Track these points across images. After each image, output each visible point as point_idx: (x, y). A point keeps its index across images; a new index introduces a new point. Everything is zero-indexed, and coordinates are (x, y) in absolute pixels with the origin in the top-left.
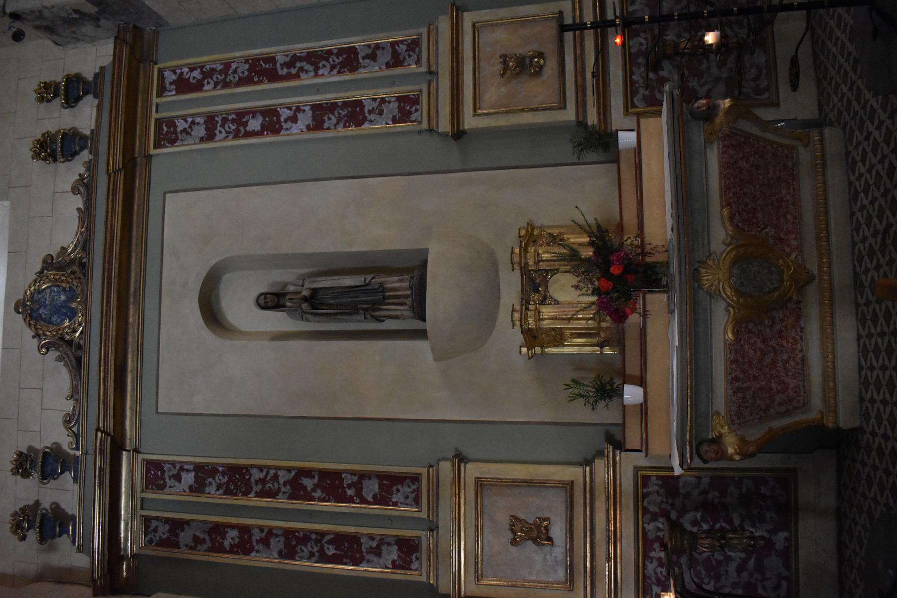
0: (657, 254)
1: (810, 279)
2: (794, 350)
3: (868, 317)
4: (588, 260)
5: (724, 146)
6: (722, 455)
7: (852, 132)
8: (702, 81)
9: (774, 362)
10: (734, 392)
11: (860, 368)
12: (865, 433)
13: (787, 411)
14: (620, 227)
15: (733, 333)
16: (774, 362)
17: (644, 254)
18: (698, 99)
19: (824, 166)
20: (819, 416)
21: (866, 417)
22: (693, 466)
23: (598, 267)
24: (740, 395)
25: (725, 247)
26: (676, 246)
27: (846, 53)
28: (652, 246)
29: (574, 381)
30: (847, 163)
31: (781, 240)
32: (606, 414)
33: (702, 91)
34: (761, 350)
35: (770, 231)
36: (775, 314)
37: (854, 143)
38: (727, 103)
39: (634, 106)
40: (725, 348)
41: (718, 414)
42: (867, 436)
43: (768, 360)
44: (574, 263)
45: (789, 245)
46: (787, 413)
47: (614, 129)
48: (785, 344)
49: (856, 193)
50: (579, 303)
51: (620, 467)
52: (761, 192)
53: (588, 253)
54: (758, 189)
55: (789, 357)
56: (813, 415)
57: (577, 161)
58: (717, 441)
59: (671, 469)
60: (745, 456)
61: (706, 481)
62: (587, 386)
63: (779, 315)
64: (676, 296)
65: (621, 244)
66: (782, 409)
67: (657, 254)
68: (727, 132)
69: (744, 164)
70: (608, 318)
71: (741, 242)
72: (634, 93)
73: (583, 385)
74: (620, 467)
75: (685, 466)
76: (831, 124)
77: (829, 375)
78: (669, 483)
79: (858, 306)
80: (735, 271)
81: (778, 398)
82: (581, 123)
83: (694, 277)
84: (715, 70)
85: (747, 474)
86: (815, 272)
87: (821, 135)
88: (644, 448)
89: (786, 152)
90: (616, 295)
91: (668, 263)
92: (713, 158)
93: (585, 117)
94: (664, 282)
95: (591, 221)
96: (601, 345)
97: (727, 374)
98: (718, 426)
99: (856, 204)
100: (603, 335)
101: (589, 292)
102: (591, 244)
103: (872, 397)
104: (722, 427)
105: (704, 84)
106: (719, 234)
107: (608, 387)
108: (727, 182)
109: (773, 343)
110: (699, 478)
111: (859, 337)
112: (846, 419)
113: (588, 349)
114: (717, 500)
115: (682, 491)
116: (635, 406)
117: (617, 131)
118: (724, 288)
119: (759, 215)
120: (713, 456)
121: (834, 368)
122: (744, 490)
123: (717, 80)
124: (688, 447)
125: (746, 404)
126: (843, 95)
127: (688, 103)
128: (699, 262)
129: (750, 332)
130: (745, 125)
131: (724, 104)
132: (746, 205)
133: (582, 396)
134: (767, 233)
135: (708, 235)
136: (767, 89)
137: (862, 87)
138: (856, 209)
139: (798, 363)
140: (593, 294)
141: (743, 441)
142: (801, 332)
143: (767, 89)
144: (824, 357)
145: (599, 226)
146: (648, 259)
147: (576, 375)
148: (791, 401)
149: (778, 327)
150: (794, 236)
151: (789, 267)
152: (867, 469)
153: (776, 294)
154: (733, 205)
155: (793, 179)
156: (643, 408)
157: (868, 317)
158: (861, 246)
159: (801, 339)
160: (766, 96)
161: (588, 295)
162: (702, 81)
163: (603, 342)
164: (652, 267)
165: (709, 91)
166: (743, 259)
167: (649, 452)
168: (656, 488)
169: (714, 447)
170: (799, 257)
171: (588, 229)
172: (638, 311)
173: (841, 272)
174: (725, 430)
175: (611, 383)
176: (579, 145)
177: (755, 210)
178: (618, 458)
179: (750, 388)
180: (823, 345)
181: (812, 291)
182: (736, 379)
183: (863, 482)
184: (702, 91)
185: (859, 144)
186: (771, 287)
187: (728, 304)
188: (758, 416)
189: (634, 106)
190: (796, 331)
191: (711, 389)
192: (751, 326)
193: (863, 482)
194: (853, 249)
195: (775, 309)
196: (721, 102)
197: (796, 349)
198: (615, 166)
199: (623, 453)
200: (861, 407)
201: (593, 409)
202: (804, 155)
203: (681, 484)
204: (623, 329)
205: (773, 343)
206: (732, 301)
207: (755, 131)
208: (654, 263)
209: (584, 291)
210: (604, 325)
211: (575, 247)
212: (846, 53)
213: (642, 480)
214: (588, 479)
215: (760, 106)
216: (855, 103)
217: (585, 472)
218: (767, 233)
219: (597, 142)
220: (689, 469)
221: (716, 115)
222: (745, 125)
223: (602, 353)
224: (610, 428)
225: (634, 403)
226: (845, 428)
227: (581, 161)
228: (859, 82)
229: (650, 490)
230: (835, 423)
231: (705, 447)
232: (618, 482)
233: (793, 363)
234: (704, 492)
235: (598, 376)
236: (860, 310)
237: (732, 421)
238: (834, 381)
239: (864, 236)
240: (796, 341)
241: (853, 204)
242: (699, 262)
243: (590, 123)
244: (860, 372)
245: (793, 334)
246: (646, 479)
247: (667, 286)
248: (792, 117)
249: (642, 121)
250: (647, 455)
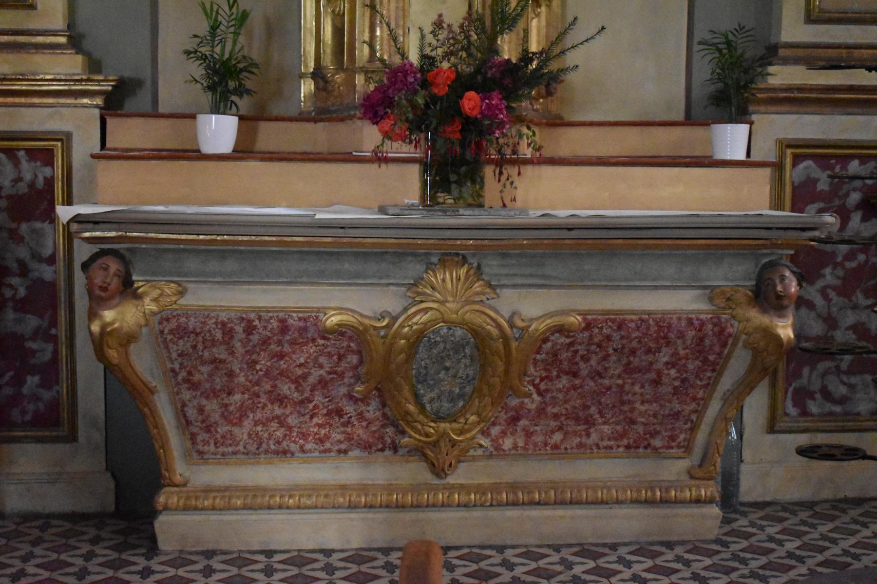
0: (499, 186)
1: (438, 471)
2: (304, 436)
3: (364, 568)
4: (494, 50)
5: (702, 324)
6: (99, 299)
7: (711, 554)
8: (832, 294)
9: (281, 400)
10: (224, 324)
11: (269, 553)
12: (148, 559)
13: (188, 423)
14: (556, 122)
15: (339, 325)
16: (281, 400)
17: (500, 163)
18: (801, 279)
19: (650, 502)
20: (178, 479)
21: (181, 560)
22: (76, 242)
23: (478, 71)
24: (219, 335)
25: (507, 316)
26: (512, 221)
27: (858, 551)
28: (515, 178)
29: (244, 16)
30: (652, 544)
31: (515, 420)
32: (177, 79)
33: (812, 293)
34: (305, 377)
35: (533, 403)
36: (374, 404)
37: (687, 556)
38: (785, 330)
39: (797, 159)
40: (311, 309)
41: (182, 293)
42: (142, 562)
43: (286, 388)
44: (488, 23)
45: (504, 433)
46: (184, 422)
47: (754, 117)
48: (315, 420)
49: (595, 556)
50: (407, 32)
51: (68, 106)
52: (609, 388)
53: (508, 48)
54: (613, 384)
55: (290, 428)
56: (180, 469)
57: (696, 40)
58: (127, 288)
59: (69, 201)
60: (99, 344)
61: (47, 272)
62: (235, 42)
63: (372, 410)
64: (416, 218)
65: (520, 120)
66: (192, 413)
67: (499, 186)
68: (730, 330)
69: (664, 357)
70: (372, 87)
71: (514, 345)
72: (822, 161)
73: (236, 34)
74: (68, 106)
75: (74, 227)
76: (726, 521)
77: (257, 500)
78: (37, 203)
79: (386, 551)
80: (459, 332)
81: (212, 406)
82: (772, 53)
83: (452, 257)
84: (850, 318)
85: (64, 351)
86: (451, 480)
87: (710, 501)
88: (106, 152)
89: (682, 437)
90: (420, 101)
91: (481, 206)
92: (682, 302)
93: (785, 61)
94: (441, 197)
95: (571, 59)
96: (318, 74)
97: (258, 311)
98: (155, 293)
99: (575, 554)
100: (339, 78)
101: (427, 51)
102: (526, 57)
103: (215, 571)
104: (155, 300)
105: (825, 296)
106: (533, 306)
107: (232, 84)
108: (632, 325)
109: (319, 399)
110: (51, 260)
111: (328, 553)
112: (172, 527)
113: (310, 47)
114: (8, 293)
115: (24, 227)
116: (195, 138)
117: (751, 123)
118: (426, 310)
119: (564, 382)
120: (98, 281)
121: (270, 508)
122: (33, 345)
123: (831, 322)
124: (113, 234)
125: (200, 347)
126: (780, 543)
127: (793, 259)
128: (479, 267)
129: (340, 358)
130: (738, 365)
131: (784, 327)
132: (585, 359)
133: (214, 28)
134: (529, 395)
135: (531, 286)
136: (804, 413)
137: (792, 574)
138: (566, 553)
139: (278, 443)
140: (424, 57)
141: (129, 339)
142: (339, 451)
143: (804, 413)
144: (292, 490)
145: (562, 81)
146: (489, 171)
147: (256, 21)
148: (208, 429)
149: (349, 409)
150: (521, 444)
151: (461, 432)
152: (80, 561)
153: (411, 408)
154: (586, 334)
155: (628, 447)
156: (194, 154)
157: (364, 568)
158: (498, 559)
159: (325, 451)
160: (792, 411)
161: (421, 48)
162: (832, 294)
163: (324, 78)
164: (474, 177)
165: (810, 305)
166: (486, 354)
167: (103, 163)
168: (28, 177)
169: (115, 283)
170: (480, 452)
171: (557, 50)
172: (388, 142)
173: (450, 526)
174: (149, 305)
175: (241, 91)
176: (728, 43)
177: (575, 375)
178: (85, 101)
179: (232, 353)
180: (313, 489)
181: (412, 472)
182: (250, 329)
183: (55, 556)
184: (812, 293)
185: (687, 563)
186: (425, 400)
187: (395, 319)
188: (177, 366)
189: (797, 159)
190: (340, 442)
191: (230, 280)
192: (354, 359)
193: (55, 556)
194: (491, 547)
195: (384, 405)
196: (790, 321)
197: (306, 440)
198: (680, 116)
199: (97, 112)
200: (197, 553)
201: (188, 53)
202: (674, 468)
203: (38, 225)
204: (351, 118)
205: (319, 399)
206: (402, 326)
207: (727, 382)
208: (482, 178)
209: (430, 38)
210: (359, 80)
211: (521, 25)
212: (858, 551)
213: (44, 149)
214: (40, 39)
215: (773, 398)
216: (763, 560)
217: (55, 33)
218: (529, 395)
219: (731, 90)
220: (69, 237)
221: (764, 311)
222: (738, 365)
223: (302, 76)
224: (148, 83)
225: (200, 144)
226: (157, 524)
227: (696, 48)
228: (803, 570)
229: (25, 165)
230: (166, 508)
231: (114, 266)
232: (36, 100)
233: (279, 434)
234: (24, 270)
235: (256, 65)
236: (379, 555)
237: (168, 320)
238: (245, 507)
239: (515, 565)
240: (321, 441)
241: (575, 549)
242: (479, 267)
243: (771, 69)
244: (262, 552)
245: (336, 436)
246: (46, 157)
247: (435, 202)
248: (747, 454)
249: (767, 172)
250: (93, 156)
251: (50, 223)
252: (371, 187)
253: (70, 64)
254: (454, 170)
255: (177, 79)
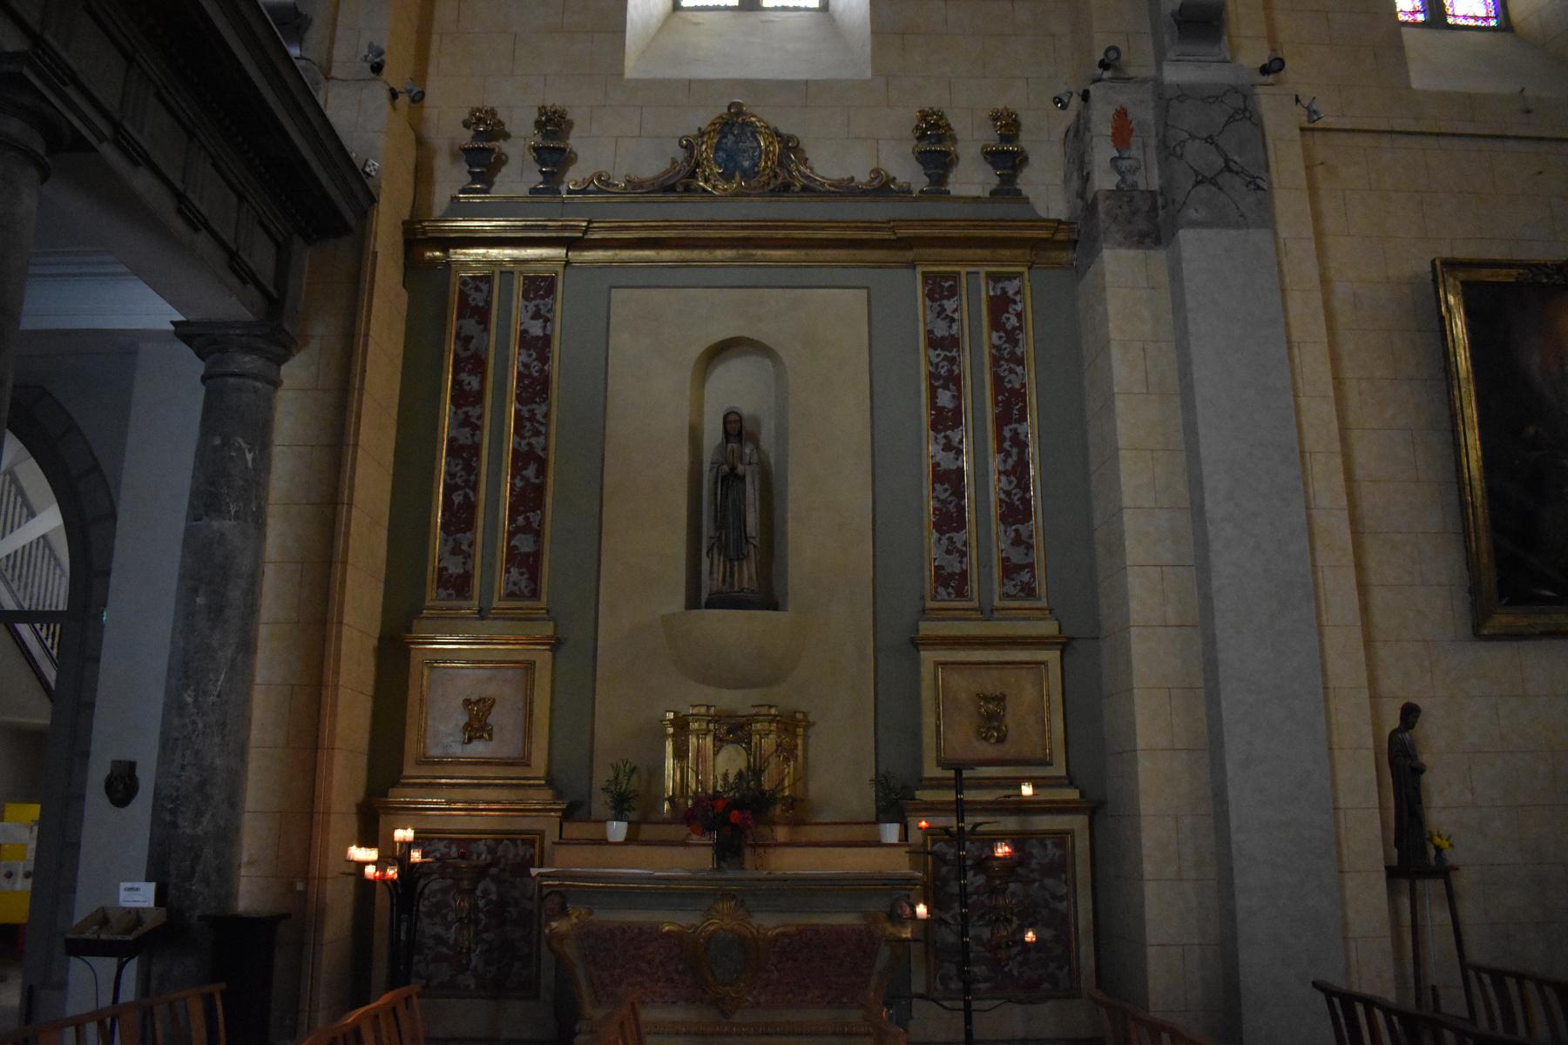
6: (551, 917)
41: (591, 913)
43: (643, 966)
61: (1063, 906)
83: (727, 896)
88: (563, 841)
92: (849, 919)
94: (723, 864)
106: (769, 923)
110: (531, 899)
146: (748, 852)
149: (676, 977)
168: (521, 853)
174: (574, 920)
219: (894, 801)
246: (532, 843)
251: (479, 323)
252: (690, 860)
253: (547, 794)
254: (728, 851)
255: (601, 804)
